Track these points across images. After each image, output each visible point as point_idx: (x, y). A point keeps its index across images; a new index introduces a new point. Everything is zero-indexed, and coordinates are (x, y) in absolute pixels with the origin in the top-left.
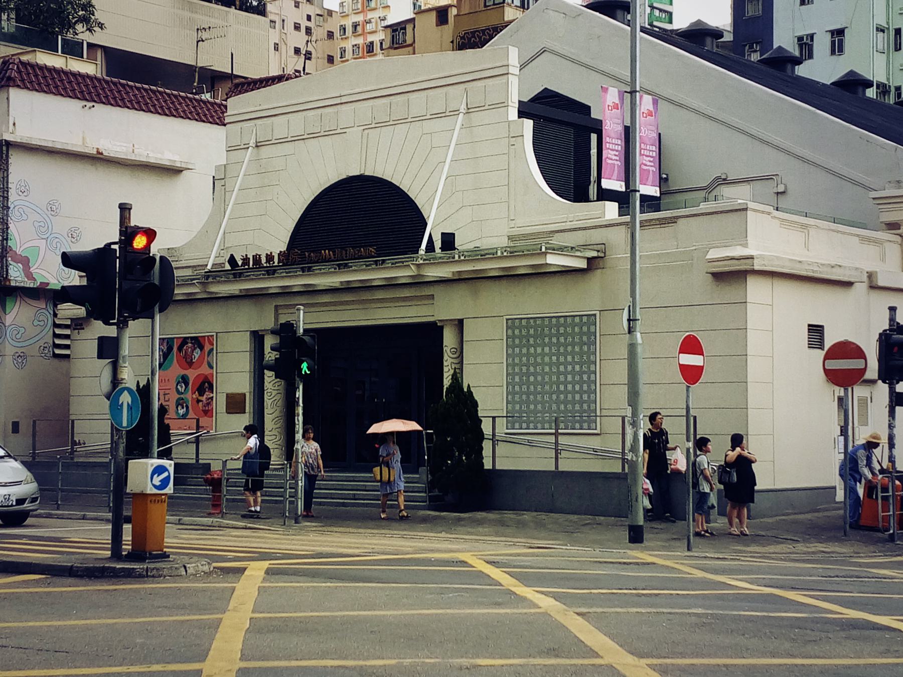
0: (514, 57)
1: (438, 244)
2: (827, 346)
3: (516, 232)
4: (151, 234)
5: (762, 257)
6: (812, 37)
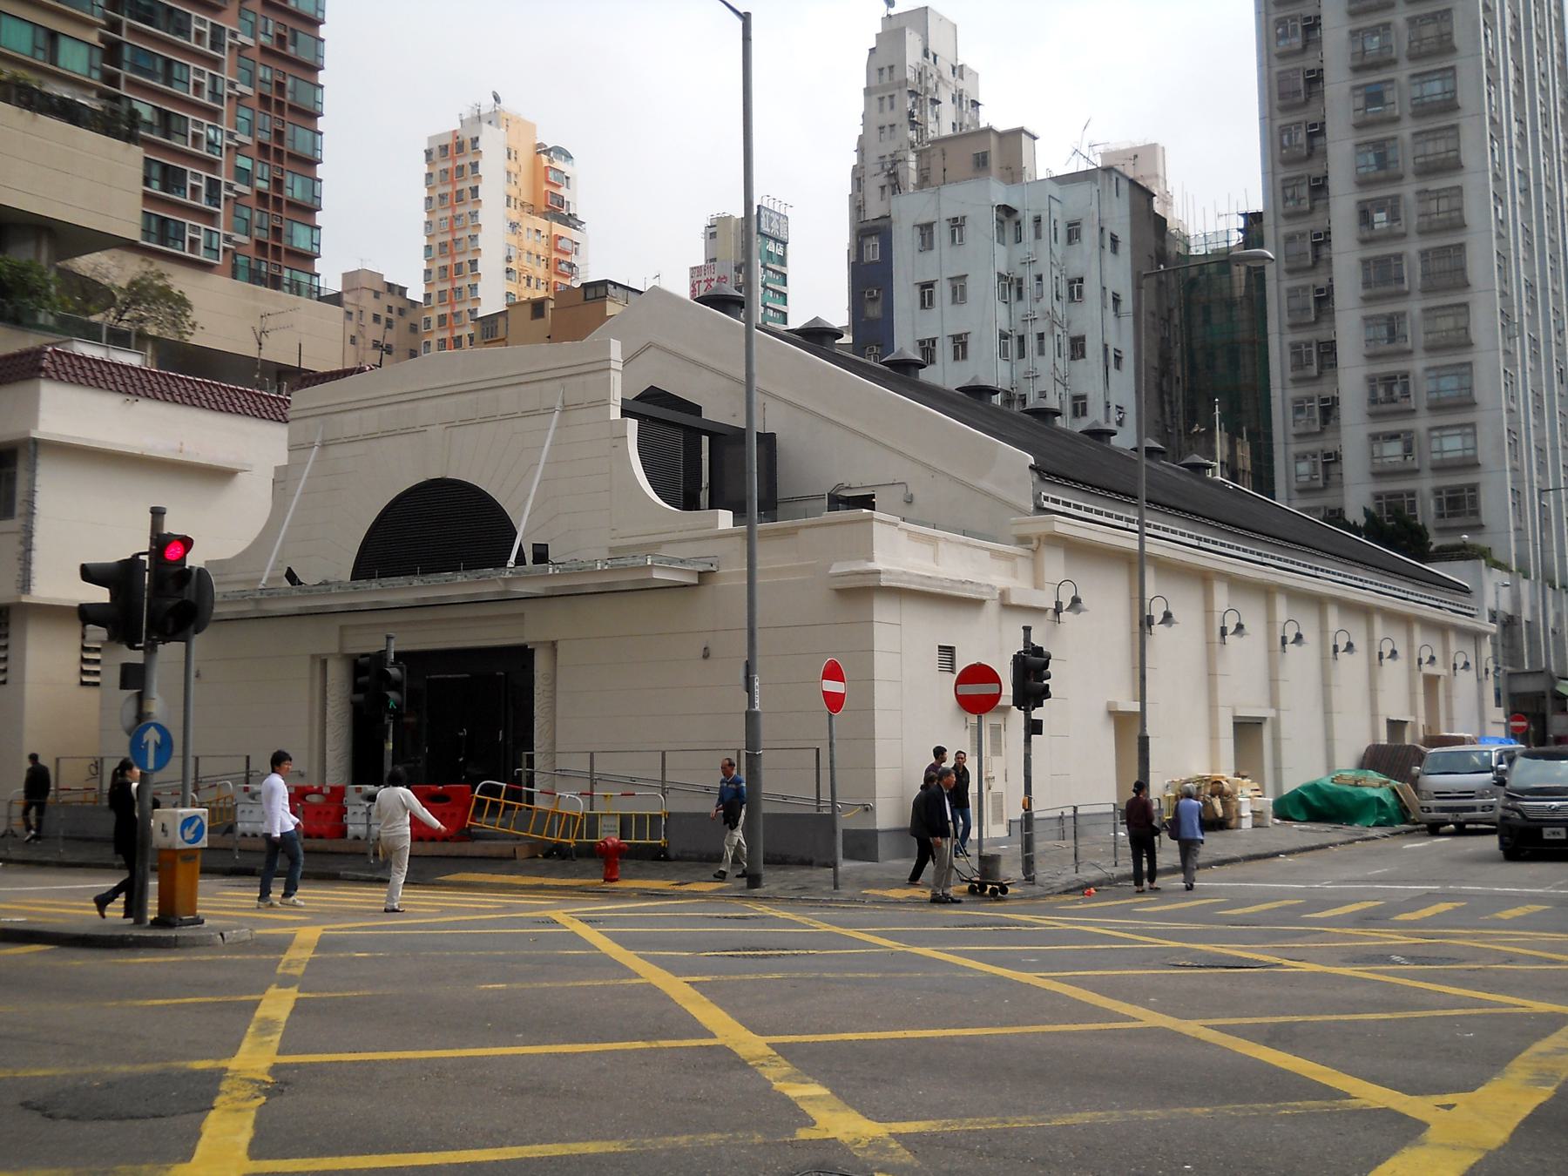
0: (616, 350)
1: (529, 557)
2: (959, 669)
3: (618, 543)
4: (187, 543)
5: (889, 572)
6: (934, 341)
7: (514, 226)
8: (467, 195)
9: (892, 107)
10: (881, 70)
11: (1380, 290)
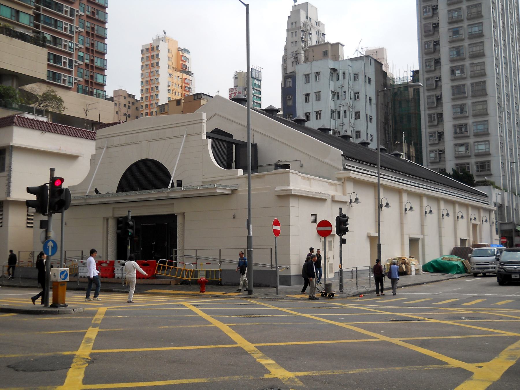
0: (204, 116)
1: (175, 185)
2: (318, 222)
3: (205, 180)
4: (62, 180)
5: (295, 190)
6: (310, 113)
7: (170, 75)
8: (155, 65)
9: (296, 36)
10: (292, 23)
11: (458, 96)
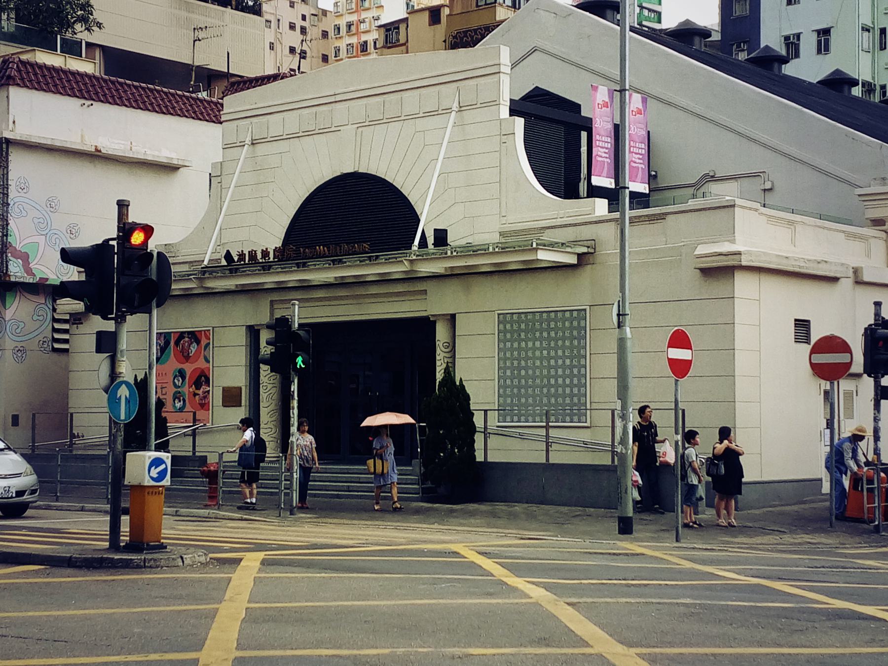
0: (505, 56)
1: (431, 240)
2: (814, 340)
3: (507, 228)
4: (148, 230)
5: (749, 253)
6: (798, 36)
